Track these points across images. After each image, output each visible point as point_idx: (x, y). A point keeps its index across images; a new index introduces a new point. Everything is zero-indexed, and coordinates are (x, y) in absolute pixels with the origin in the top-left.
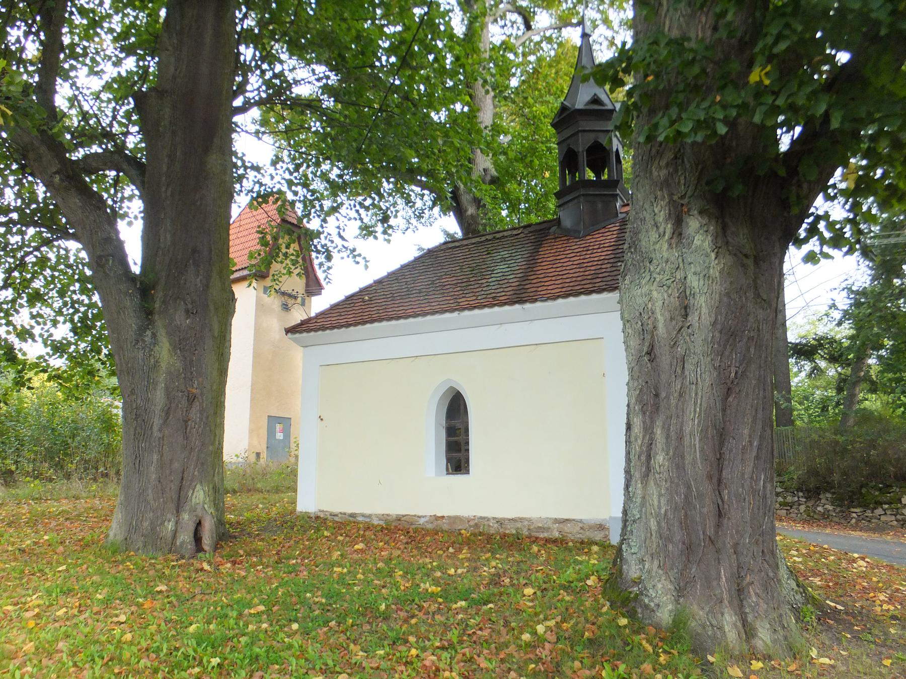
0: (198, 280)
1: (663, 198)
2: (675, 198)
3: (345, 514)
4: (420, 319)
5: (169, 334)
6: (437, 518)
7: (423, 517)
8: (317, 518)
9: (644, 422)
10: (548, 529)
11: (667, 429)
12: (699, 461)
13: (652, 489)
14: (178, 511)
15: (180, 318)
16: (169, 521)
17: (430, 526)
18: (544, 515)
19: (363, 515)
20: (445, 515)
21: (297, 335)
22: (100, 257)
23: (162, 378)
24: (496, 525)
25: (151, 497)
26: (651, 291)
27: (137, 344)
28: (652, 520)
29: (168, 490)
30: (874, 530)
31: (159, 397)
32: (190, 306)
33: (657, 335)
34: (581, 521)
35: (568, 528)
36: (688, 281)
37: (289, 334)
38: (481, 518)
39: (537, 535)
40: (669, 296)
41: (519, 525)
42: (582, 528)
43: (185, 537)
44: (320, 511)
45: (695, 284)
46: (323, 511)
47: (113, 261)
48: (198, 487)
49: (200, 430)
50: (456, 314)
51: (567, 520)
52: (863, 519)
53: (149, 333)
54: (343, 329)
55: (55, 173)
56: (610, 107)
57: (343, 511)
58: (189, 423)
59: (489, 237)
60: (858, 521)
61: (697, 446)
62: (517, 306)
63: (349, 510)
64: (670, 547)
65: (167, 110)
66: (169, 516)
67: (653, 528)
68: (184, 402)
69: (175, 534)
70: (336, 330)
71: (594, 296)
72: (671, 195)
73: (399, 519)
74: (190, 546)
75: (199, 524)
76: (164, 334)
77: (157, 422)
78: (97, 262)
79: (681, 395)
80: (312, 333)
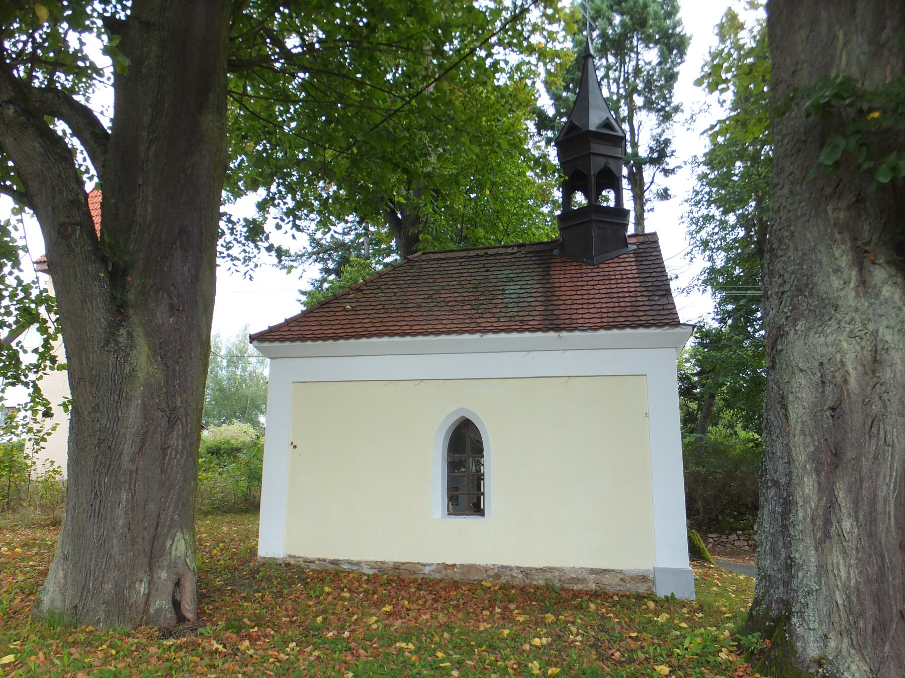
0: (186, 268)
1: (844, 242)
2: (859, 243)
3: (324, 560)
4: (431, 338)
5: (147, 334)
6: (446, 566)
7: (429, 565)
8: (288, 565)
9: (819, 484)
10: (582, 581)
11: (855, 491)
12: (893, 529)
13: (836, 557)
14: (150, 569)
15: (162, 315)
16: (141, 581)
17: (438, 576)
18: (578, 564)
19: (349, 562)
20: (458, 563)
21: (267, 344)
22: (63, 225)
23: (138, 391)
24: (520, 576)
25: (115, 551)
26: (840, 341)
27: (107, 345)
28: (837, 593)
29: (140, 540)
30: (731, 554)
31: (133, 415)
32: (175, 301)
33: (848, 390)
34: (621, 572)
35: (606, 579)
36: (880, 334)
37: (255, 342)
38: (503, 567)
39: (570, 586)
40: (863, 348)
41: (549, 576)
42: (622, 580)
43: (162, 603)
44: (290, 556)
45: (889, 338)
46: (294, 557)
47: (81, 232)
48: (179, 535)
49: (183, 461)
50: (477, 336)
51: (605, 570)
52: (719, 544)
53: (123, 331)
54: (330, 342)
55: (9, 102)
56: (621, 134)
57: (321, 556)
58: (169, 451)
59: (480, 252)
60: (714, 545)
61: (892, 513)
62: (552, 334)
63: (330, 555)
64: (861, 624)
65: (154, 48)
66: (141, 574)
67: (840, 602)
68: (164, 423)
69: (148, 599)
70: (320, 342)
71: (641, 331)
72: (854, 239)
73: (397, 567)
74: (169, 615)
75: (178, 584)
76: (141, 334)
77: (128, 449)
78: (59, 232)
79: (876, 458)
80: (287, 344)
